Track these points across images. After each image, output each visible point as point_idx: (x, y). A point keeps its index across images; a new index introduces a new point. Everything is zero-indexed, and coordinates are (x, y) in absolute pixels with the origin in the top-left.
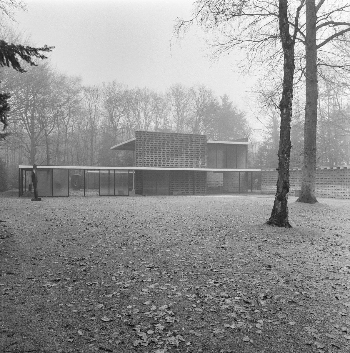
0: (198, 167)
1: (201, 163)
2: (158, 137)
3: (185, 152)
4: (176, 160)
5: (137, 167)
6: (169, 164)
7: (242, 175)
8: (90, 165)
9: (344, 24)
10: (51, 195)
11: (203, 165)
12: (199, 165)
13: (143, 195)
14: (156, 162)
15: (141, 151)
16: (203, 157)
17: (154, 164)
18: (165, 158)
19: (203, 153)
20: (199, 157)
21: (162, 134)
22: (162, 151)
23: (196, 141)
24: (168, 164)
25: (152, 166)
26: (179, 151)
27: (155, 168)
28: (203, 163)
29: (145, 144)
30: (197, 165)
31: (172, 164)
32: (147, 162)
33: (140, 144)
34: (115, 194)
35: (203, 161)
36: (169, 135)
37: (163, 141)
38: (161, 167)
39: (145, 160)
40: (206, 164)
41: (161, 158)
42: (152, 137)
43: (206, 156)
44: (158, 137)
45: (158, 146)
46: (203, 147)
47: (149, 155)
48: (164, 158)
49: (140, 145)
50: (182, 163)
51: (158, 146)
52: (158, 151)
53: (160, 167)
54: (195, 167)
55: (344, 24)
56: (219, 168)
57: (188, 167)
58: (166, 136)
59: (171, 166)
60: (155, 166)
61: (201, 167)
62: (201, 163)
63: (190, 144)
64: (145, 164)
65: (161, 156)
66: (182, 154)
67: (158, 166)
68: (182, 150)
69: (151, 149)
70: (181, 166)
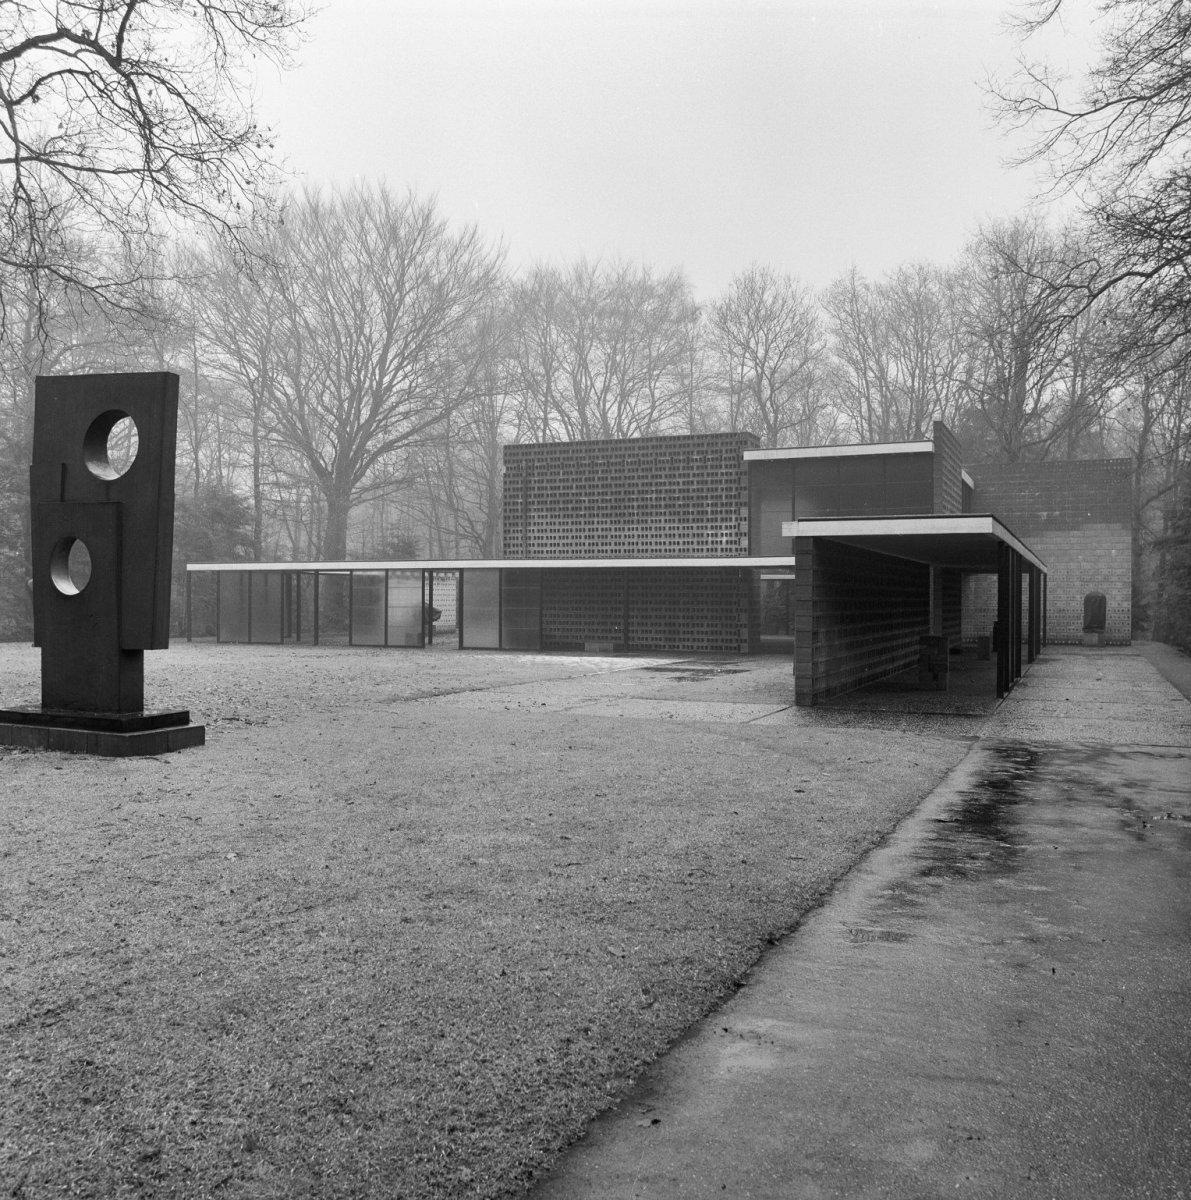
0: (712, 553)
1: (724, 539)
2: (572, 459)
3: (663, 503)
4: (631, 533)
5: (508, 559)
6: (608, 548)
7: (276, 581)
8: (428, 557)
9: (136, 93)
10: (383, 643)
11: (734, 547)
12: (719, 547)
13: (219, 642)
14: (578, 541)
15: (519, 507)
16: (734, 517)
17: (570, 549)
18: (595, 526)
19: (734, 501)
20: (719, 516)
21: (584, 448)
22: (583, 505)
23: (705, 460)
24: (604, 548)
25: (553, 555)
26: (643, 499)
27: (512, 562)
28: (733, 538)
29: (532, 485)
30: (710, 546)
31: (617, 548)
32: (536, 542)
33: (516, 486)
34: (389, 644)
35: (733, 531)
36: (649, 444)
37: (667, 466)
38: (580, 558)
39: (531, 534)
40: (745, 543)
41: (582, 527)
42: (643, 455)
43: (744, 512)
44: (572, 459)
45: (572, 488)
46: (733, 477)
47: (544, 521)
48: (591, 527)
49: (518, 489)
50: (654, 540)
51: (572, 488)
52: (570, 506)
53: (577, 558)
54: (697, 553)
55: (136, 93)
56: (760, 556)
57: (677, 553)
58: (597, 453)
59: (616, 554)
60: (643, 554)
61: (727, 553)
62: (724, 539)
63: (681, 472)
64: (532, 549)
65: (582, 520)
66: (654, 511)
67: (557, 554)
68: (654, 496)
69: (549, 499)
70: (570, 555)
